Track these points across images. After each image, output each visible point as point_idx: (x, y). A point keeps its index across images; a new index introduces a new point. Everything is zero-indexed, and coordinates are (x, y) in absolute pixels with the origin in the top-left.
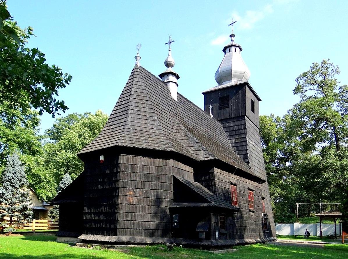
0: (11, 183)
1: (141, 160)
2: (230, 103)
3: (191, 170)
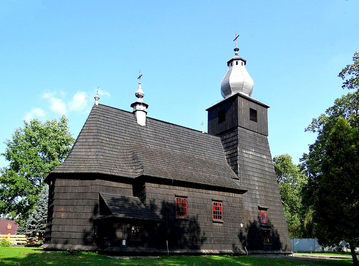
0: (42, 206)
1: (73, 182)
2: (226, 115)
3: (130, 186)
